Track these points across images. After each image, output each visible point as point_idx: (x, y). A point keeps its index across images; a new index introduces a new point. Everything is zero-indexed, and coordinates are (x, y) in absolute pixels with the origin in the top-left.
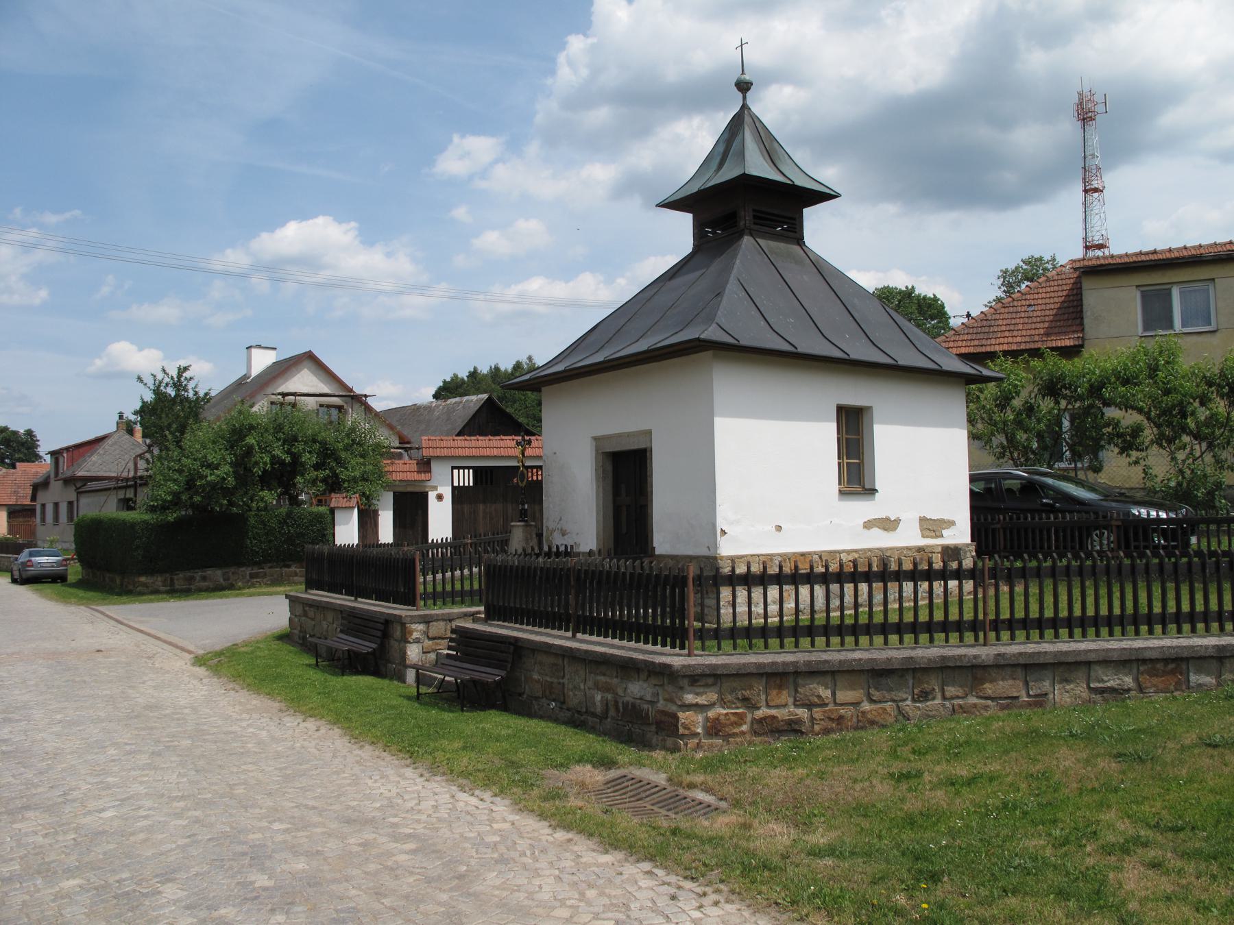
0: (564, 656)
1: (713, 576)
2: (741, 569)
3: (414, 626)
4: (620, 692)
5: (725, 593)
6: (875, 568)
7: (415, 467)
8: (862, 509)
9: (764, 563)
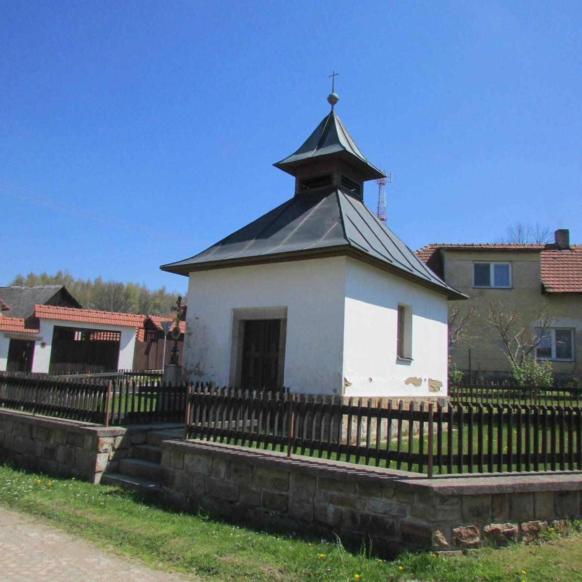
0: (23, 424)
1: (334, 409)
2: (406, 408)
3: (105, 439)
4: (359, 506)
5: (345, 417)
6: (333, 403)
7: (23, 323)
8: (406, 371)
9: (389, 400)
